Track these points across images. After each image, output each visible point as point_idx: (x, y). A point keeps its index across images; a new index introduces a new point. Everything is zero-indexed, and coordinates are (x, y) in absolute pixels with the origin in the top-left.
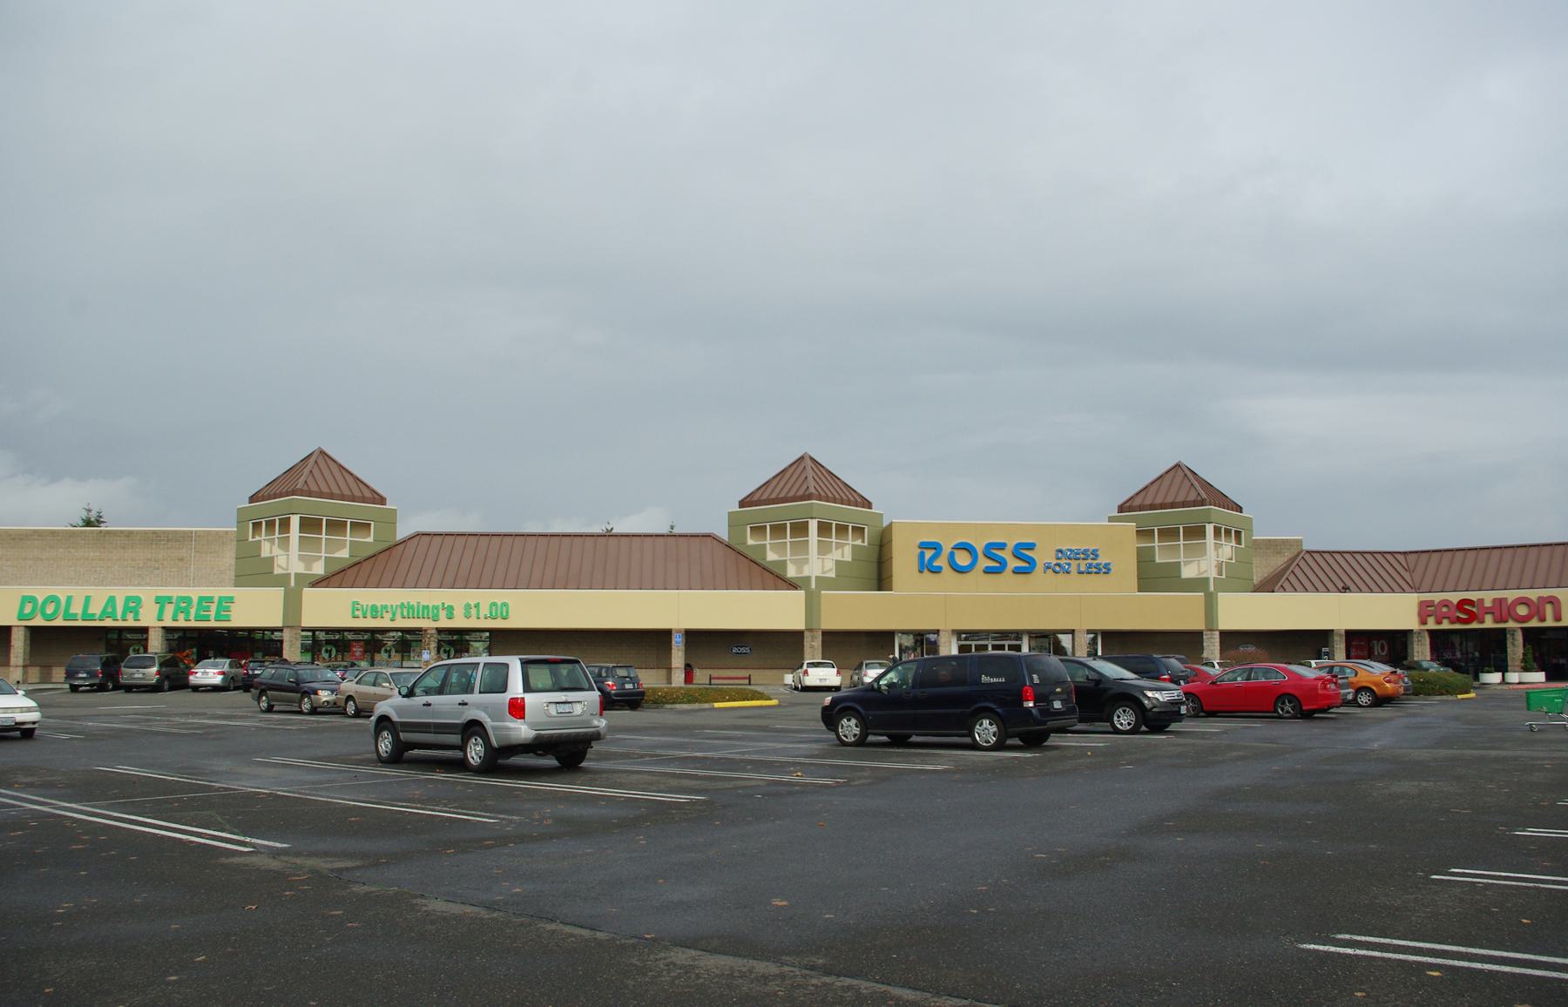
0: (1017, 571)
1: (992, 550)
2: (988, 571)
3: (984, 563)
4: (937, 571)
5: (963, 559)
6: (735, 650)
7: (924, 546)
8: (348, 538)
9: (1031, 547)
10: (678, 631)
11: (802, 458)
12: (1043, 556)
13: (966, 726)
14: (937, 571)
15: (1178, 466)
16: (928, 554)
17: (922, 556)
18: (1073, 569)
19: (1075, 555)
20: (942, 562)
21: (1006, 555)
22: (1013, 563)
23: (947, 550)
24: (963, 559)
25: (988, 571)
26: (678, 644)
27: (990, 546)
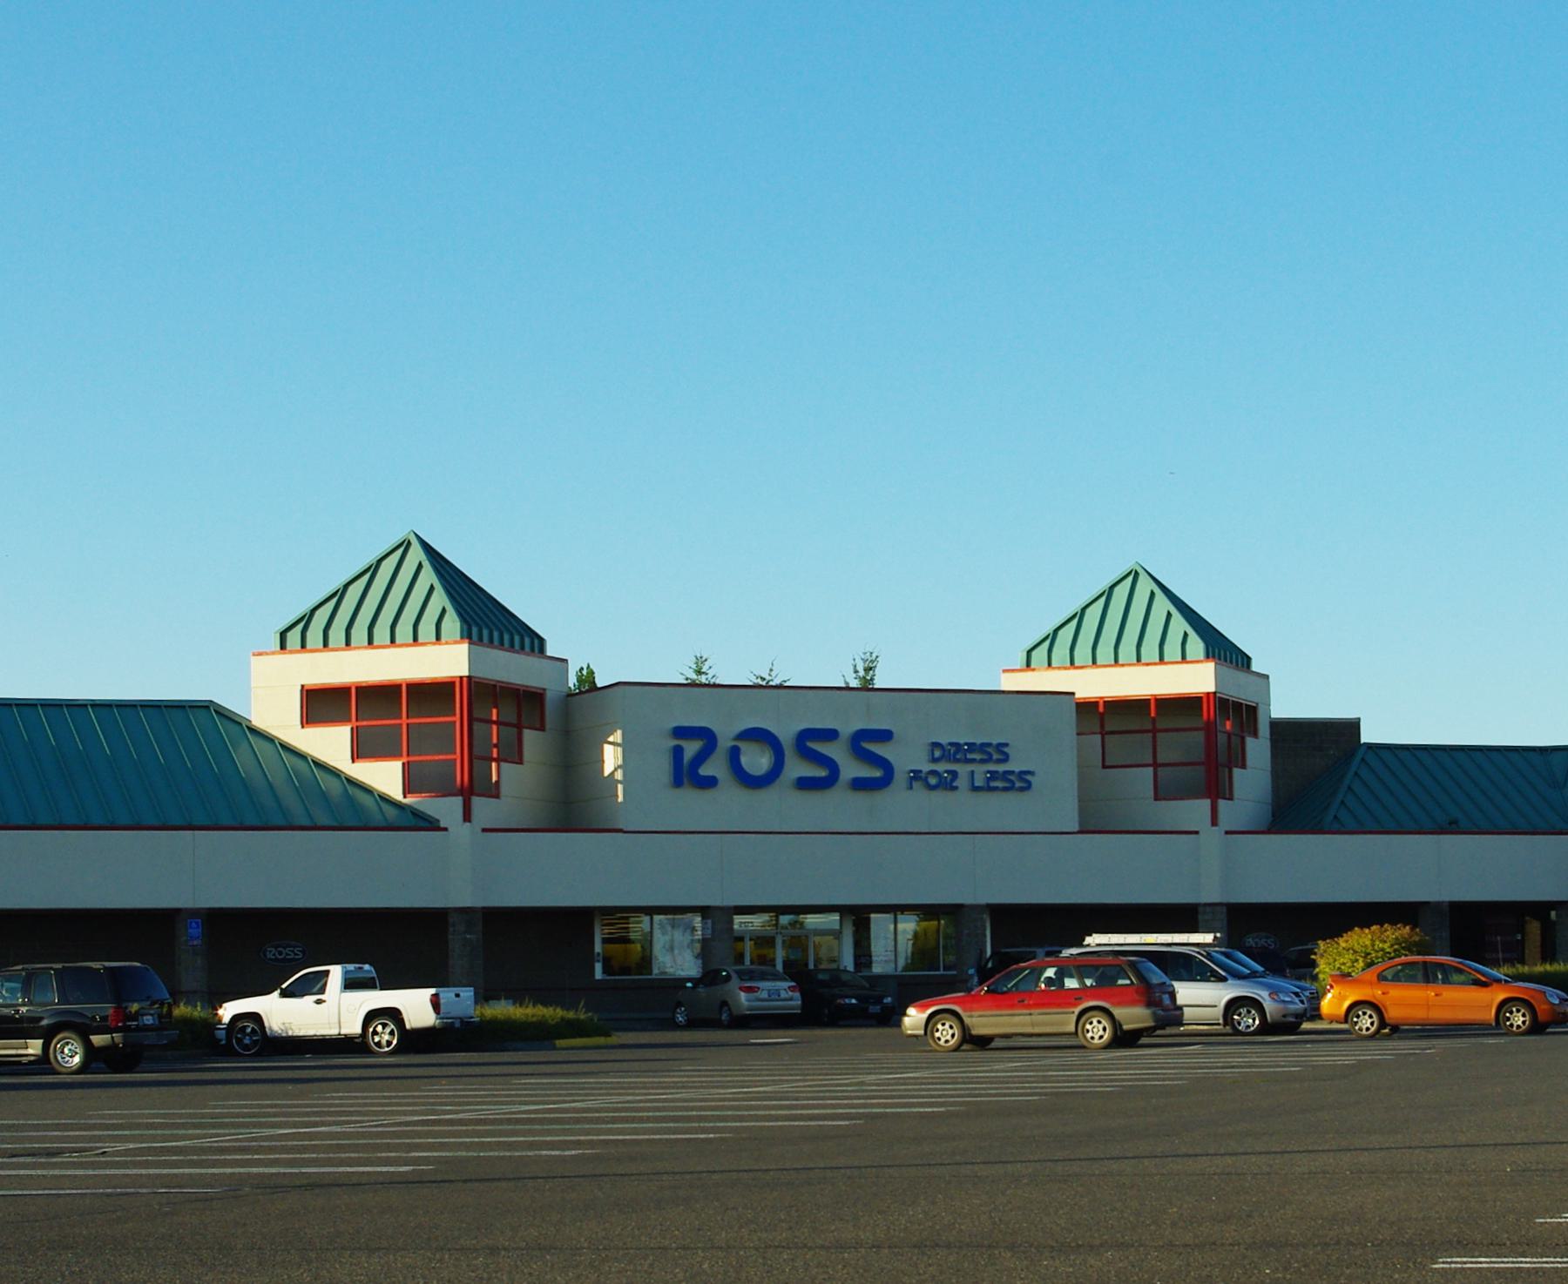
0: (859, 785)
1: (865, 742)
2: (804, 784)
3: (797, 768)
4: (710, 782)
5: (757, 760)
6: (271, 953)
7: (681, 732)
8: (404, 720)
9: (885, 736)
10: (194, 913)
11: (405, 545)
12: (906, 756)
13: (892, 1017)
14: (710, 782)
15: (1267, 677)
16: (691, 748)
17: (678, 752)
18: (962, 782)
19: (956, 752)
20: (714, 767)
21: (835, 751)
22: (851, 769)
23: (725, 743)
24: (757, 760)
25: (804, 784)
26: (193, 934)
27: (806, 735)
